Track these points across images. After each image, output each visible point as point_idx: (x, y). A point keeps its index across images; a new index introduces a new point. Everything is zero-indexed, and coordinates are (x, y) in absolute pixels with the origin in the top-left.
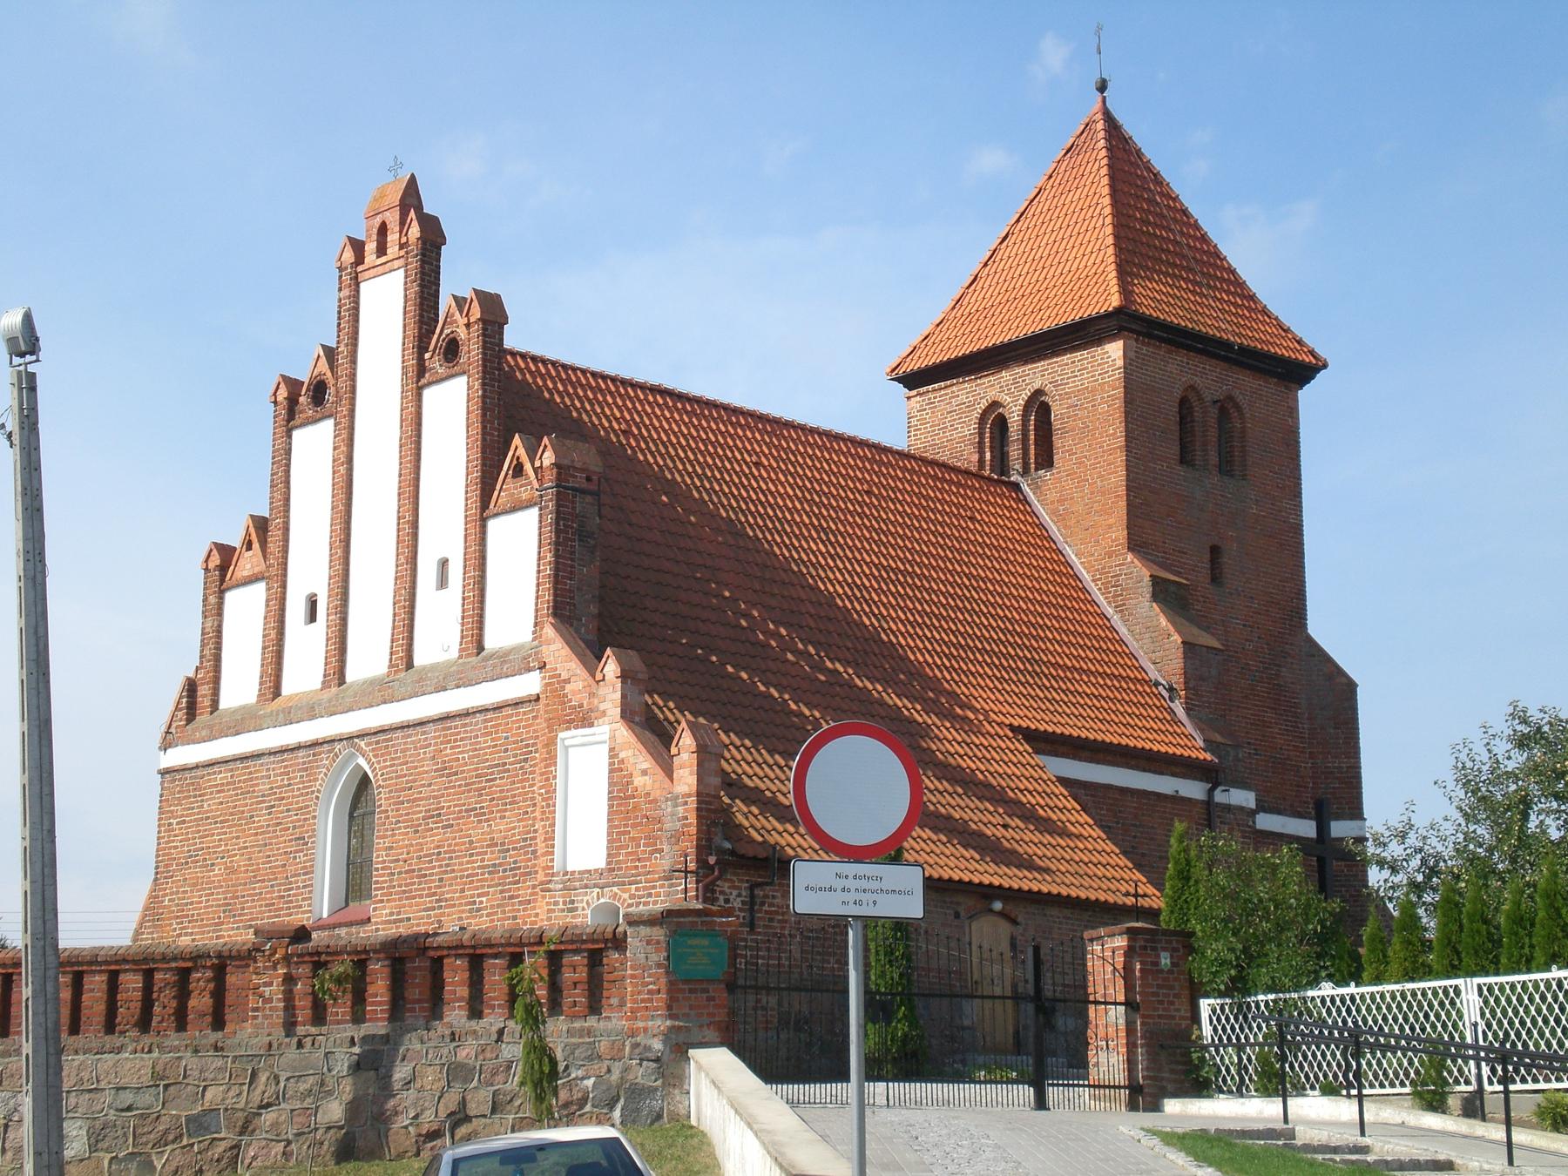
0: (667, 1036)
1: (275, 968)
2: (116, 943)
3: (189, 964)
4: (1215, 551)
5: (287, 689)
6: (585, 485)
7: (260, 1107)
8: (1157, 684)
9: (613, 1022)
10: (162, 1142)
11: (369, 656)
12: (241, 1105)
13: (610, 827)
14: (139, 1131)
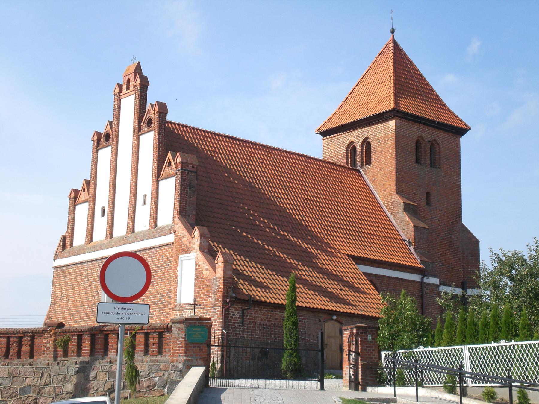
0: (184, 363)
1: (51, 337)
2: (36, 326)
3: (22, 335)
4: (428, 194)
5: (94, 240)
6: (192, 169)
7: (44, 385)
8: (404, 240)
9: (166, 357)
10: (11, 397)
11: (120, 230)
12: (38, 385)
13: (195, 289)
14: (3, 393)
